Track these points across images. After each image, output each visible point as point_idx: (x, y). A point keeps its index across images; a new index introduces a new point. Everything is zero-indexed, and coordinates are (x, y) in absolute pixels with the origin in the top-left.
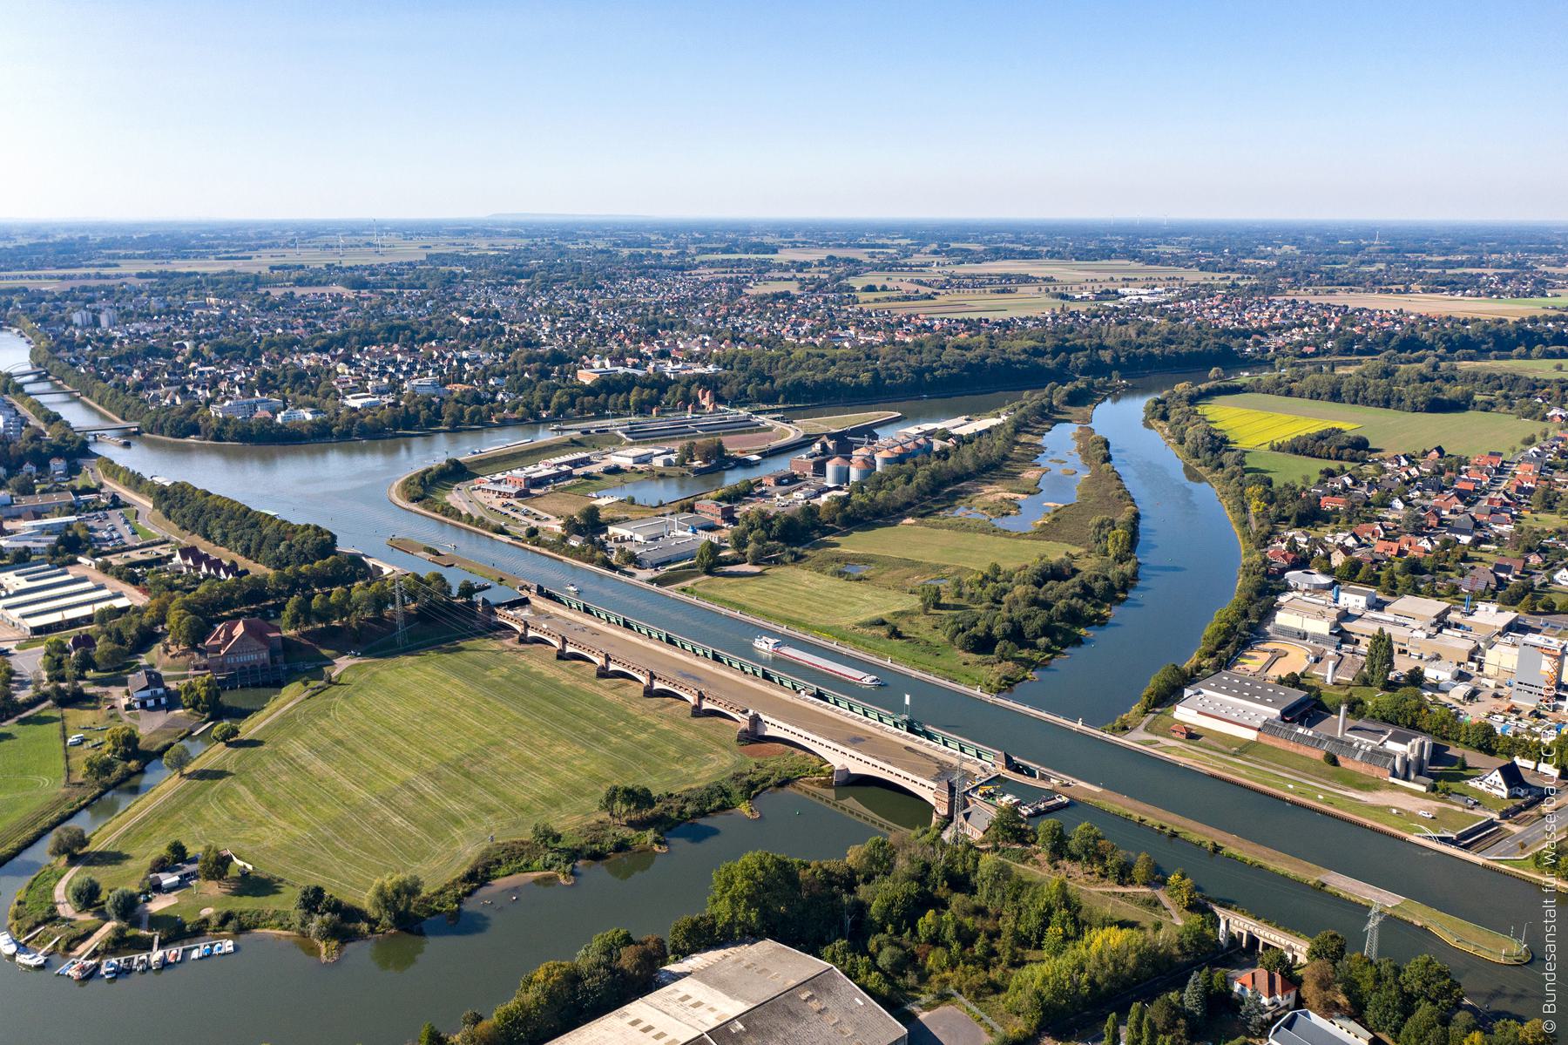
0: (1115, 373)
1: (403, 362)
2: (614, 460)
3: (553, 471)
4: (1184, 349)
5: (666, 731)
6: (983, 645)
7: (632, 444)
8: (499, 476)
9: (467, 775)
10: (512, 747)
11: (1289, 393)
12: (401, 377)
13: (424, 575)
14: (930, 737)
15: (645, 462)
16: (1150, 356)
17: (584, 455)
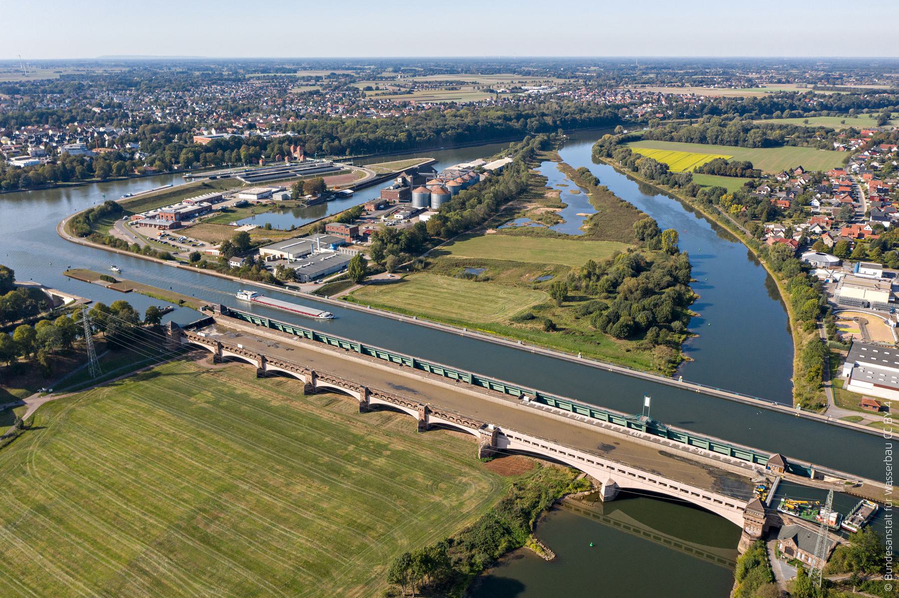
0: (560, 130)
1: (55, 135)
2: (242, 197)
3: (196, 207)
4: (593, 115)
5: (403, 452)
6: (634, 332)
7: (251, 186)
8: (152, 213)
9: (205, 540)
10: (246, 492)
11: (672, 139)
12: (54, 144)
13: (110, 304)
14: (670, 435)
15: (266, 198)
16: (574, 120)
17: (217, 194)
